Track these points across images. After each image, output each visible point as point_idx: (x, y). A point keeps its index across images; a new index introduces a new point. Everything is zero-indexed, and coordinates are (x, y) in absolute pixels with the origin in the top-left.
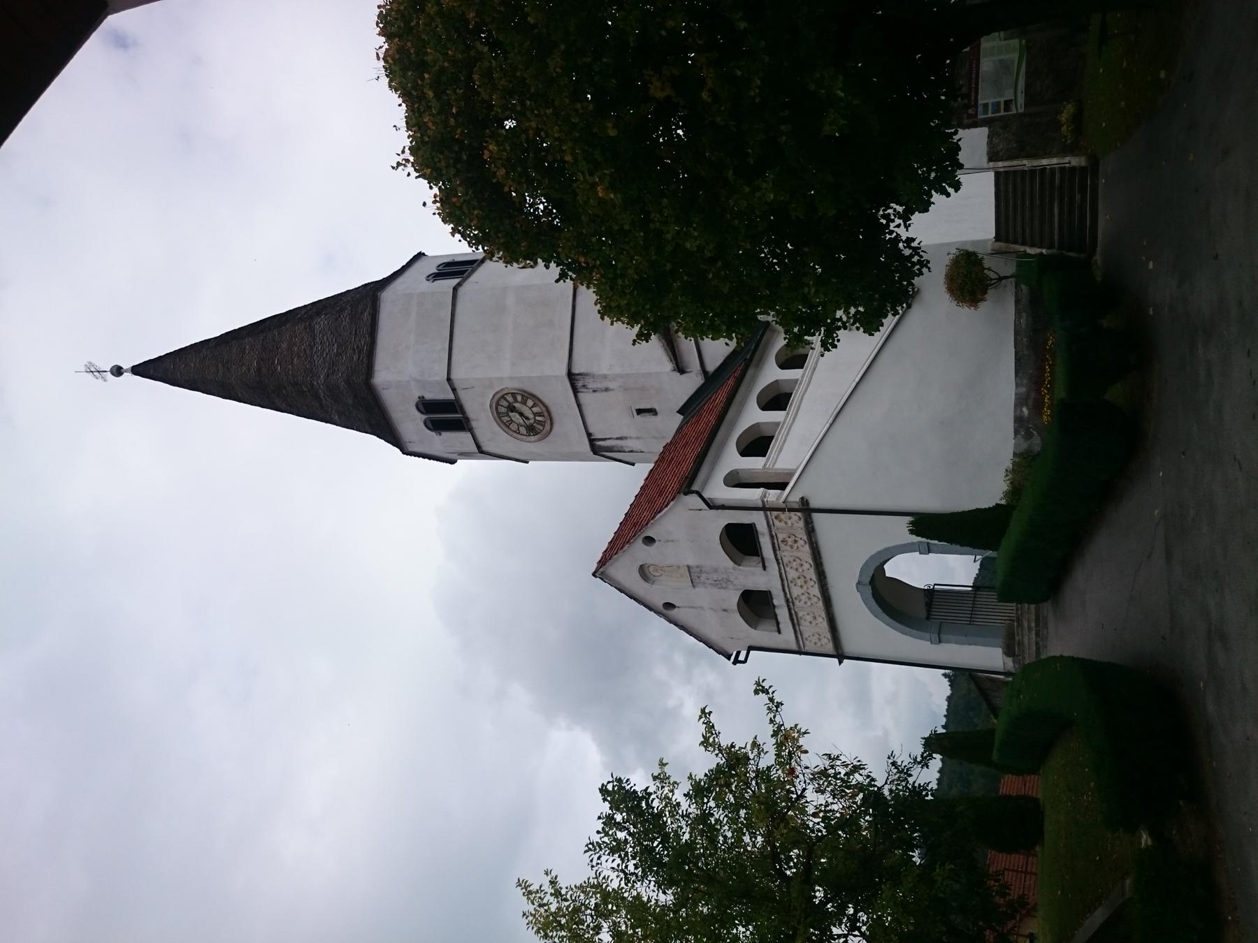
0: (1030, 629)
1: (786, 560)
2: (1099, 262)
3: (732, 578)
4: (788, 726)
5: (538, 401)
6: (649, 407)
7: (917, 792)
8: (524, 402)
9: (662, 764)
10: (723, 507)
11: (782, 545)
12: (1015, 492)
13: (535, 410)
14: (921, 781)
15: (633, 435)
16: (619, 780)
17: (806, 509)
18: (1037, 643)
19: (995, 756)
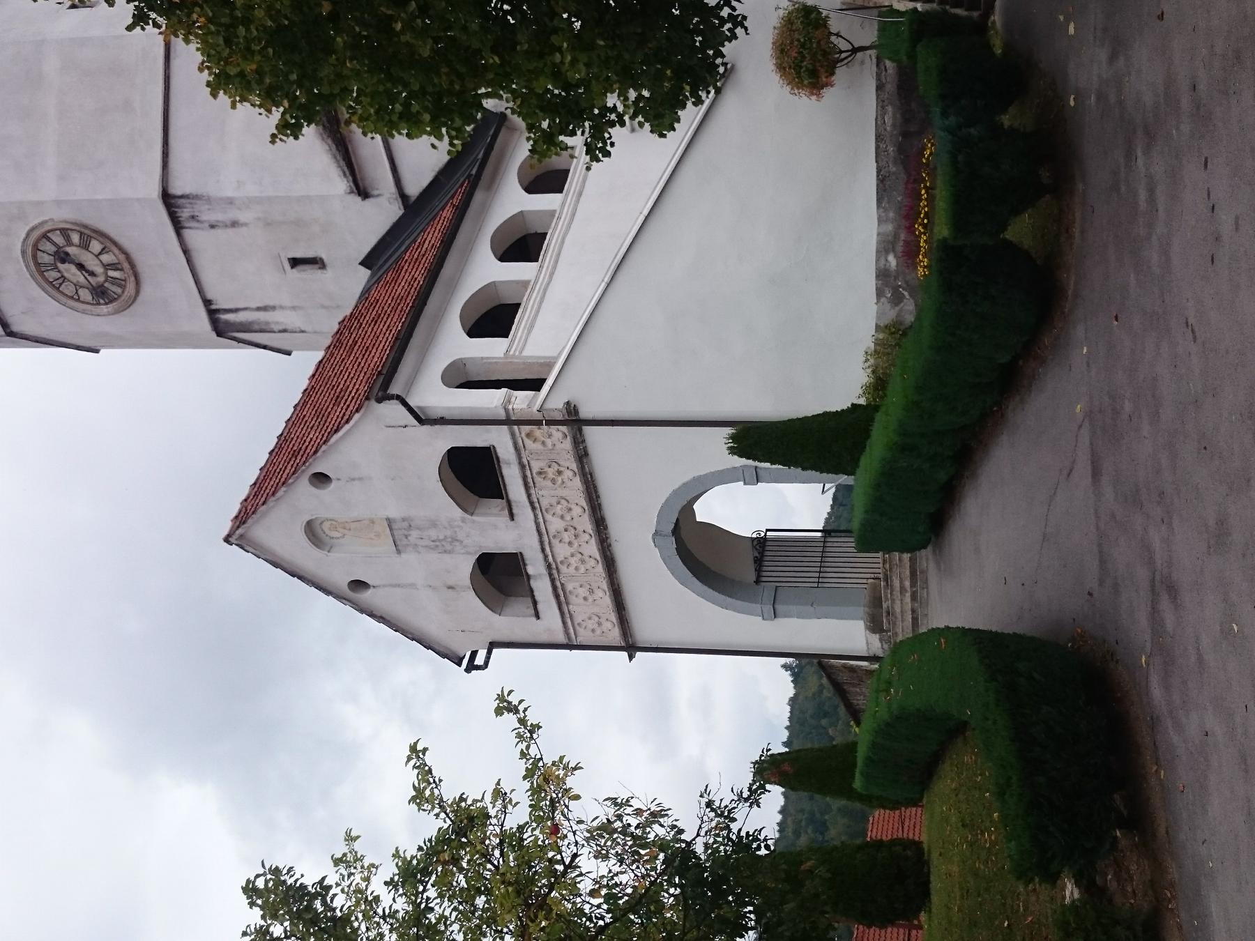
0: (903, 589)
1: (545, 503)
2: (999, 25)
3: (460, 536)
4: (548, 760)
5: (109, 242)
6: (310, 254)
7: (745, 845)
8: (85, 246)
9: (350, 838)
10: (442, 421)
11: (538, 479)
12: (879, 385)
13: (106, 258)
14: (750, 828)
15: (287, 303)
16: (276, 871)
17: (574, 420)
18: (913, 611)
19: (858, 784)
